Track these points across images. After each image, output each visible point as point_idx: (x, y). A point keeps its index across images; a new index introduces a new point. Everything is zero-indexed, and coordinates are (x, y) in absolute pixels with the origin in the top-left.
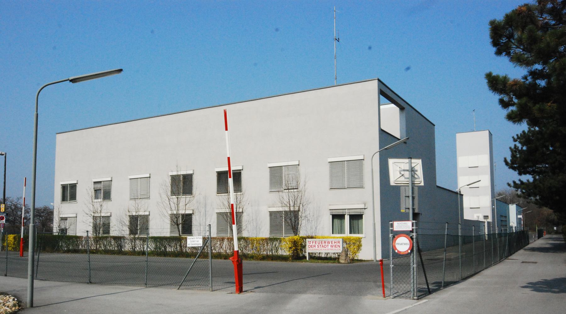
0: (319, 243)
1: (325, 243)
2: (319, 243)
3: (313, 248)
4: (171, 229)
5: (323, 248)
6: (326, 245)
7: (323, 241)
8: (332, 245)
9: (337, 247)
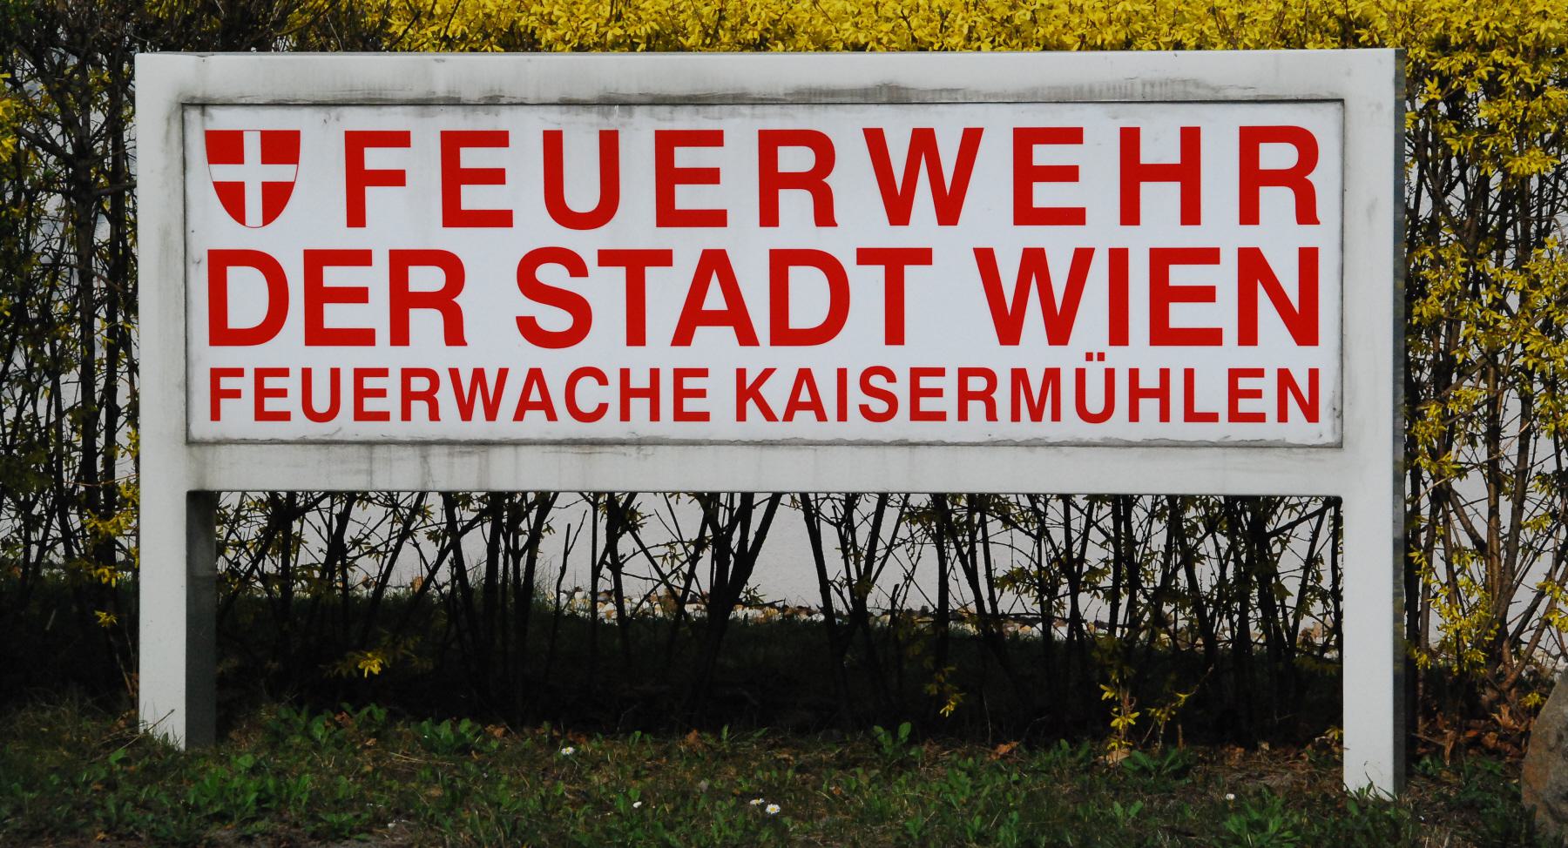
0: (582, 194)
1: (795, 204)
2: (582, 194)
3: (382, 354)
4: (1396, 64)
5: (714, 343)
6: (840, 243)
7: (742, 131)
8: (1058, 245)
9: (1223, 313)
